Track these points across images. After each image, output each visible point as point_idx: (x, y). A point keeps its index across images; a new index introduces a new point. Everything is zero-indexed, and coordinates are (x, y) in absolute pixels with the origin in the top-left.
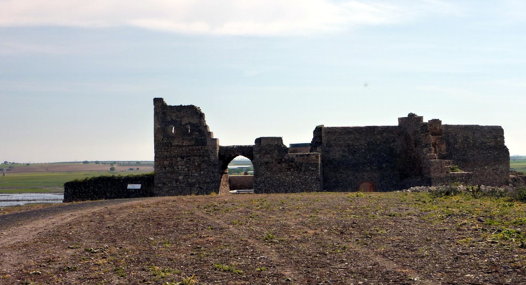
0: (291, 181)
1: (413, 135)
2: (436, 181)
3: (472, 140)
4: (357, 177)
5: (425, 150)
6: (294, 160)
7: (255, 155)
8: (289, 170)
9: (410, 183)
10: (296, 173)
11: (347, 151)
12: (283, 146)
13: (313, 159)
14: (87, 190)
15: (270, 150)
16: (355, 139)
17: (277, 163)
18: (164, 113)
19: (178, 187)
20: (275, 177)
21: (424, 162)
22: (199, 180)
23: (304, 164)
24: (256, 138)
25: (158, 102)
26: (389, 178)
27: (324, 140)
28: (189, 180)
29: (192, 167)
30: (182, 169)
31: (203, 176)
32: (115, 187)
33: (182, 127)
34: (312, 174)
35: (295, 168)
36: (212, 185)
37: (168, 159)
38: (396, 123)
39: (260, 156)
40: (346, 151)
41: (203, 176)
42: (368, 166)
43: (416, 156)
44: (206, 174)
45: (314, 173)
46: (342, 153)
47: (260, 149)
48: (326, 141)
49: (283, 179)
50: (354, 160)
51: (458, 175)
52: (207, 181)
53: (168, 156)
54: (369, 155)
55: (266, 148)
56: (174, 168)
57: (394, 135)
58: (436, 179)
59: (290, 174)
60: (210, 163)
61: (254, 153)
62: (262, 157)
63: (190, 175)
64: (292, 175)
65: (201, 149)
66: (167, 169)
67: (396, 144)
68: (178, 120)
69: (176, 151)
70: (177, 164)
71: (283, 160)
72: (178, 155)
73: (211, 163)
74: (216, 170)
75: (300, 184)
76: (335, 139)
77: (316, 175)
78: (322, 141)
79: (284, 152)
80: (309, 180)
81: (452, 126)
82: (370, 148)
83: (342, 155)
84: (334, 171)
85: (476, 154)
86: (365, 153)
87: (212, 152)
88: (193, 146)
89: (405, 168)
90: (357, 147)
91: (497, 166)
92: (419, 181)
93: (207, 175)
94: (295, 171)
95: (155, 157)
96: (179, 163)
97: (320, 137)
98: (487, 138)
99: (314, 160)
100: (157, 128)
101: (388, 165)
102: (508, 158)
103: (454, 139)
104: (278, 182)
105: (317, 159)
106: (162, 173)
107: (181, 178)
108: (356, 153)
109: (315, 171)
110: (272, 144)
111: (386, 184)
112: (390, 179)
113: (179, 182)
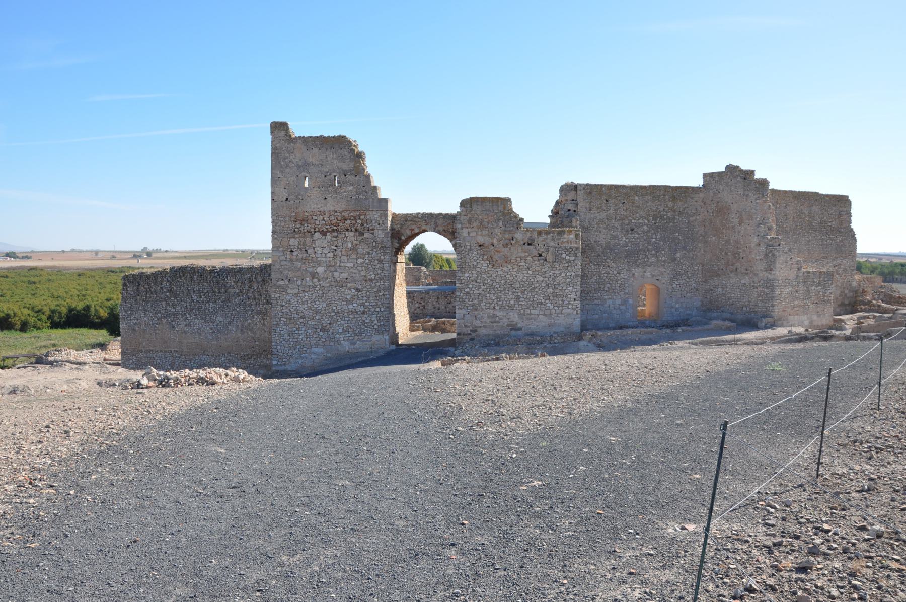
10: (538, 265)
14: (159, 288)
17: (501, 245)
22: (354, 275)
25: (279, 128)
26: (686, 278)
29: (341, 251)
30: (324, 255)
31: (362, 267)
32: (205, 284)
36: (378, 284)
37: (296, 236)
38: (698, 182)
40: (617, 228)
41: (362, 267)
42: (653, 255)
49: (512, 276)
50: (629, 245)
52: (370, 277)
54: (654, 236)
59: (526, 267)
60: (374, 243)
63: (338, 264)
64: (529, 268)
66: (295, 253)
70: (314, 245)
74: (387, 257)
86: (648, 231)
90: (636, 221)
91: (839, 261)
92: (745, 284)
93: (370, 266)
95: (276, 233)
96: (318, 243)
104: (503, 282)
106: (286, 261)
107: (320, 270)
113: (317, 278)
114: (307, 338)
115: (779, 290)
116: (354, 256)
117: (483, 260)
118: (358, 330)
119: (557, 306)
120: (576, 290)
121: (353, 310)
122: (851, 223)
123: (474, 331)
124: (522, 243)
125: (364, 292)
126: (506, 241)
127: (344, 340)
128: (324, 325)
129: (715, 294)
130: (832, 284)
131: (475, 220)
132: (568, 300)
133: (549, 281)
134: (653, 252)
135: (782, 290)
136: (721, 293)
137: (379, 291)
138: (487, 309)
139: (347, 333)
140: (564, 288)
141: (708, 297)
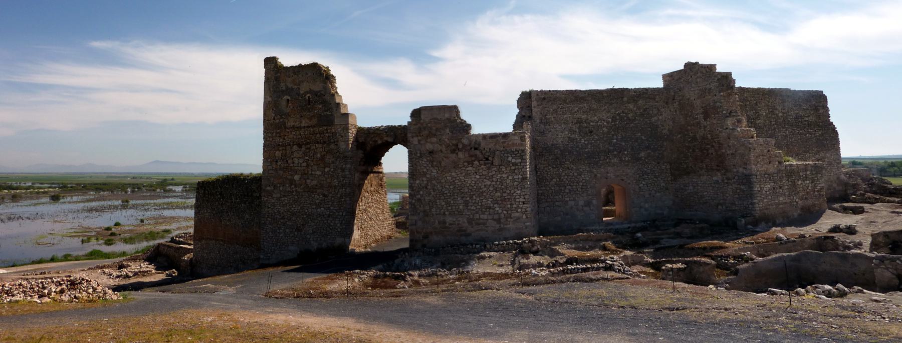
0: (475, 184)
1: (698, 98)
2: (762, 180)
3: (782, 112)
4: (596, 175)
5: (729, 122)
6: (479, 145)
7: (411, 139)
8: (471, 163)
9: (696, 185)
10: (484, 169)
11: (577, 130)
12: (459, 121)
13: (515, 142)
15: (437, 130)
16: (590, 110)
17: (449, 151)
18: (277, 79)
19: (293, 192)
20: (446, 177)
21: (730, 144)
23: (497, 153)
24: (411, 112)
27: (536, 113)
28: (308, 181)
33: (300, 98)
34: (514, 170)
35: (482, 160)
36: (340, 190)
37: (280, 149)
39: (419, 141)
43: (709, 136)
44: (332, 172)
45: (518, 169)
46: (568, 134)
47: (420, 129)
48: (539, 114)
49: (460, 180)
50: (589, 147)
51: (798, 167)
53: (280, 144)
55: (429, 125)
56: (287, 163)
57: (656, 103)
58: (760, 175)
60: (338, 154)
61: (409, 135)
62: (422, 142)
63: (310, 173)
64: (476, 173)
65: (325, 131)
66: (279, 163)
67: (660, 118)
68: (295, 87)
69: (291, 136)
70: (292, 157)
71: (460, 146)
72: (293, 142)
73: (340, 154)
75: (491, 189)
76: (556, 111)
77: (521, 173)
78: (532, 114)
79: (461, 131)
80: (508, 181)
81: (749, 90)
82: (617, 126)
83: (569, 138)
84: (555, 166)
85: (790, 135)
87: (342, 136)
88: (314, 126)
89: (684, 159)
91: (822, 154)
94: (481, 165)
96: (295, 154)
97: (529, 107)
98: (804, 109)
99: (516, 144)
100: (267, 102)
101: (649, 153)
102: (837, 141)
103: (755, 110)
105: (523, 141)
107: (297, 177)
108: (592, 134)
109: (519, 164)
110: (439, 118)
111: (647, 186)
112: (655, 177)
114: (285, 237)
115: (758, 186)
116: (322, 165)
117: (432, 166)
118: (325, 232)
119: (505, 210)
120: (524, 193)
121: (321, 214)
122: (829, 117)
123: (426, 237)
124: (469, 148)
125: (330, 198)
126: (453, 147)
127: (313, 240)
128: (299, 225)
129: (686, 193)
130: (822, 177)
131: (425, 129)
132: (517, 203)
133: (496, 184)
134: (615, 153)
135: (762, 186)
136: (692, 191)
137: (341, 197)
138: (437, 214)
139: (315, 234)
140: (512, 192)
141: (680, 196)
